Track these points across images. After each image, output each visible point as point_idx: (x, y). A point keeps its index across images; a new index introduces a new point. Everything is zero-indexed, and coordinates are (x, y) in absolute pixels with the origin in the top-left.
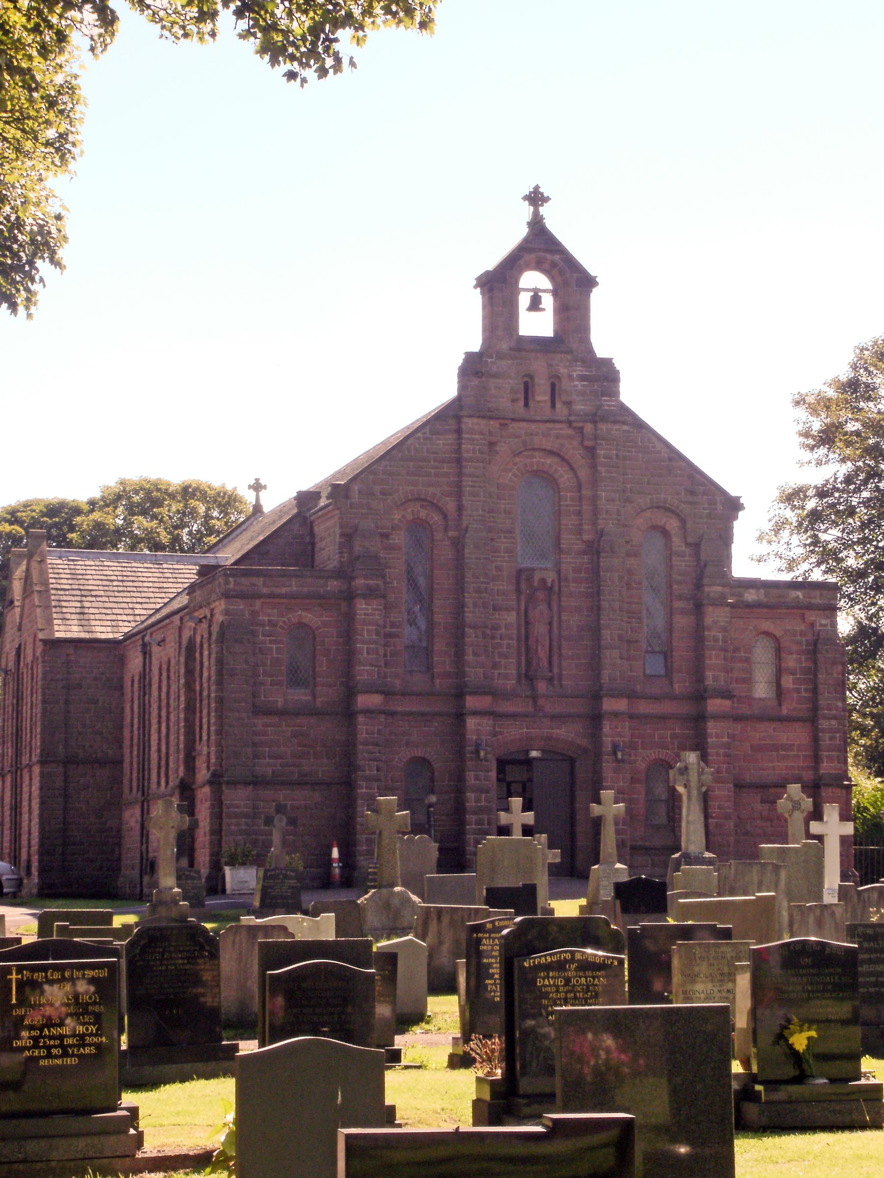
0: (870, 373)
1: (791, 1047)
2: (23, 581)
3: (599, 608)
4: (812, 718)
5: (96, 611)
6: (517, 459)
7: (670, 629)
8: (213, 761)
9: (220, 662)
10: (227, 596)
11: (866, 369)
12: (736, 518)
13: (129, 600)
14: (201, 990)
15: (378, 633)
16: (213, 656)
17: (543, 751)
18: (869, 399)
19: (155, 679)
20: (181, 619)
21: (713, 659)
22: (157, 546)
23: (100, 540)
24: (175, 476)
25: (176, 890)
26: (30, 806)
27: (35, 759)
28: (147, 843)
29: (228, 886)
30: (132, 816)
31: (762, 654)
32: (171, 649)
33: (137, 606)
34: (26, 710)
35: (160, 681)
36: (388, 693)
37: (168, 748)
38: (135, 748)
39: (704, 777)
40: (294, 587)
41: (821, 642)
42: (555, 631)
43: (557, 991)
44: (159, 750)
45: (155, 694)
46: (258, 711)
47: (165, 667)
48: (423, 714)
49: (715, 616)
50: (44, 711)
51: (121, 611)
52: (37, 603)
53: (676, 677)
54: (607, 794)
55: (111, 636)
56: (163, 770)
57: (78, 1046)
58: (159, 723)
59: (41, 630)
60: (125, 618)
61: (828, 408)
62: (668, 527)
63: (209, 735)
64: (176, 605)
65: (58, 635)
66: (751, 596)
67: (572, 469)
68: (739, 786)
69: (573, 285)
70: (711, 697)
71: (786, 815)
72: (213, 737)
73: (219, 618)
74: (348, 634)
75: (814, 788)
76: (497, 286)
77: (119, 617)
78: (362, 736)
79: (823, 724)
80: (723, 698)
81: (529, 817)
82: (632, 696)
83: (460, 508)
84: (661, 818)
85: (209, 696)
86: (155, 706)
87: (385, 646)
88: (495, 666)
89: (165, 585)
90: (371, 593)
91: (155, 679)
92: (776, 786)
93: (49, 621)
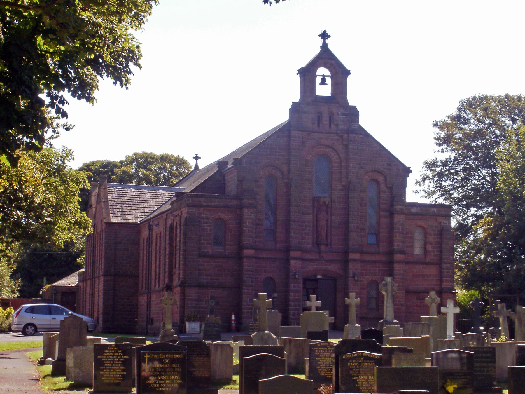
0: (466, 113)
1: (447, 391)
2: (96, 197)
3: (348, 214)
4: (439, 263)
5: (128, 211)
6: (314, 149)
7: (379, 224)
8: (181, 276)
9: (185, 234)
10: (188, 206)
11: (464, 111)
12: (408, 176)
13: (142, 206)
14: (192, 369)
15: (253, 224)
16: (182, 232)
17: (323, 275)
18: (465, 124)
19: (154, 241)
20: (167, 215)
21: (398, 237)
22: (149, 182)
23: (125, 179)
24: (158, 152)
25: (172, 330)
26: (99, 294)
27: (101, 274)
28: (150, 311)
29: (187, 330)
30: (143, 299)
31: (418, 235)
32: (161, 228)
33: (146, 209)
34: (97, 252)
35: (156, 242)
36: (256, 249)
37: (159, 271)
38: (145, 271)
39: (394, 288)
40: (216, 202)
41: (444, 231)
42: (329, 224)
43: (356, 368)
44: (155, 272)
45: (154, 247)
46: (202, 255)
47: (158, 235)
48: (271, 259)
49: (398, 219)
50: (106, 253)
51: (139, 211)
52: (103, 207)
53: (381, 245)
54: (352, 294)
55: (134, 222)
56: (157, 280)
57: (171, 384)
58: (156, 260)
59: (105, 218)
60: (140, 214)
61: (448, 128)
62: (379, 180)
63: (179, 265)
64: (163, 209)
65: (112, 221)
66: (414, 210)
67: (338, 154)
68: (408, 292)
69: (340, 74)
70: (396, 254)
71: (429, 305)
72: (181, 267)
73: (185, 215)
74: (240, 223)
75: (440, 293)
76: (307, 74)
77: (138, 214)
78: (245, 267)
79: (444, 266)
80: (401, 254)
81: (319, 303)
82: (362, 252)
83: (289, 170)
84: (373, 305)
85: (180, 249)
86: (154, 252)
87: (256, 229)
88: (303, 238)
89: (158, 200)
90: (250, 206)
91: (154, 241)
92: (423, 292)
93: (109, 216)
